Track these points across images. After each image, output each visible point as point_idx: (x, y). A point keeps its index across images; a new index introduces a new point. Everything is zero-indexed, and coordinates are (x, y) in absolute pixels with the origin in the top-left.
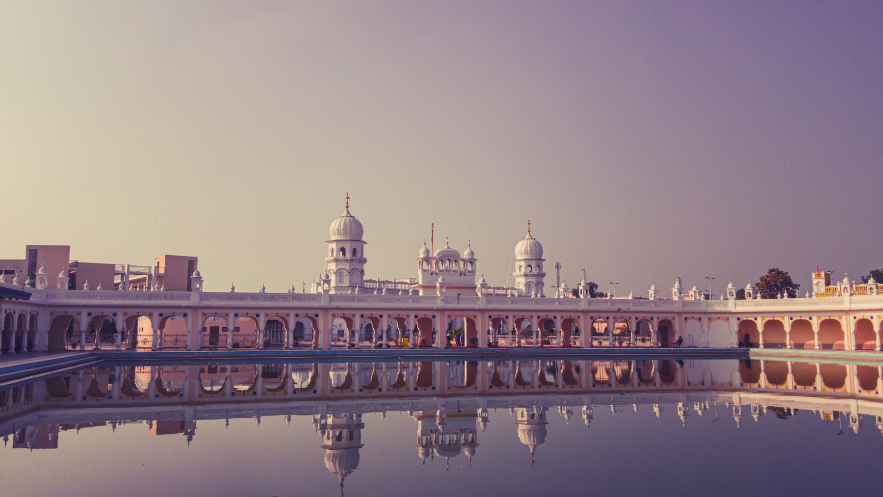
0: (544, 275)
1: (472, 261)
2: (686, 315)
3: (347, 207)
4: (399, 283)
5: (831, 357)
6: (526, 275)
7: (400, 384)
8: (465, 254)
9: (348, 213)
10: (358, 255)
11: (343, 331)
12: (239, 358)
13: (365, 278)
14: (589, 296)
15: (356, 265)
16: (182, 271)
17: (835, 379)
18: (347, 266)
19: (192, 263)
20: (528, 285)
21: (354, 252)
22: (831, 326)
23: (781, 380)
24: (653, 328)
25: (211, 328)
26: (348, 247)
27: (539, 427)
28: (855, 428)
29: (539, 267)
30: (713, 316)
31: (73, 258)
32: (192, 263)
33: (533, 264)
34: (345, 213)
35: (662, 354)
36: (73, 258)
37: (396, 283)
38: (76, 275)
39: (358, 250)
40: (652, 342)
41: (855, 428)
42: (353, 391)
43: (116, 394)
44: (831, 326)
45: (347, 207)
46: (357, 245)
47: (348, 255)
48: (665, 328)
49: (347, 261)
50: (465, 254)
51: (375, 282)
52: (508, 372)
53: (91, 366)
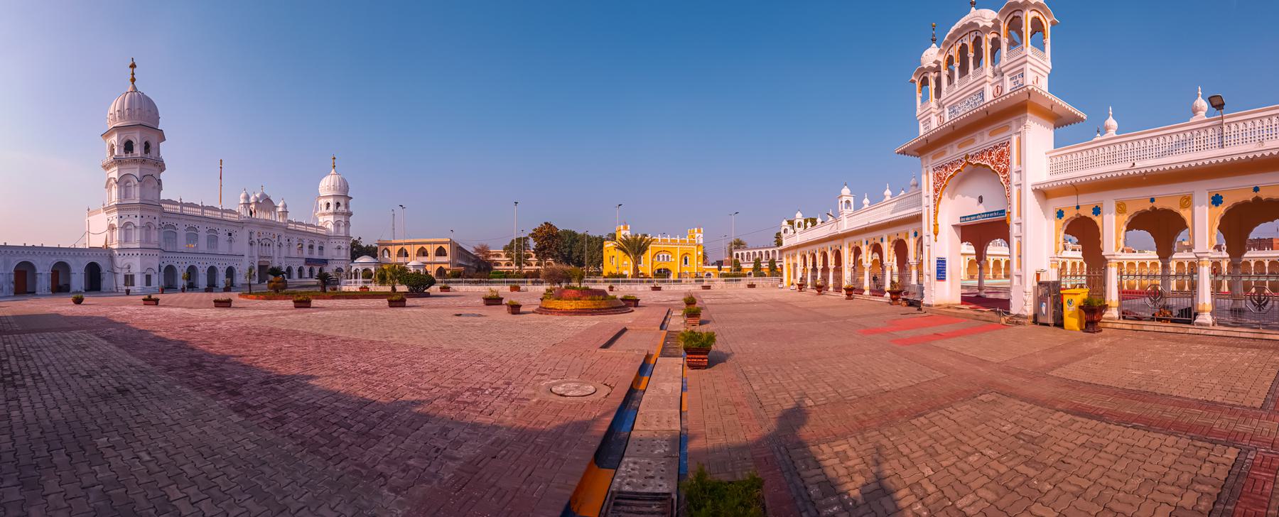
0: (350, 214)
3: (133, 80)
4: (227, 211)
6: (335, 213)
9: (134, 87)
10: (153, 154)
11: (132, 276)
13: (163, 196)
14: (700, 263)
15: (150, 169)
18: (136, 171)
20: (337, 224)
21: (147, 147)
25: (260, 267)
26: (137, 138)
29: (347, 206)
33: (342, 202)
34: (130, 88)
37: (182, 204)
39: (153, 145)
42: (1121, 208)
45: (133, 80)
46: (153, 139)
47: (138, 151)
49: (135, 161)
51: (196, 206)
53: (1206, 129)
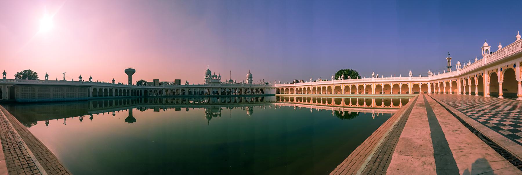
1: (220, 77)
2: (266, 88)
5: (338, 96)
7: (236, 101)
8: (218, 76)
12: (178, 96)
16: (178, 82)
17: (369, 102)
19: (180, 80)
22: (369, 87)
23: (309, 101)
24: (259, 90)
27: (251, 111)
28: (374, 117)
30: (272, 88)
31: (160, 81)
32: (180, 80)
35: (258, 95)
36: (160, 81)
38: (160, 84)
40: (260, 93)
41: (374, 117)
43: (175, 102)
44: (369, 87)
48: (262, 90)
50: (218, 76)
52: (249, 100)
